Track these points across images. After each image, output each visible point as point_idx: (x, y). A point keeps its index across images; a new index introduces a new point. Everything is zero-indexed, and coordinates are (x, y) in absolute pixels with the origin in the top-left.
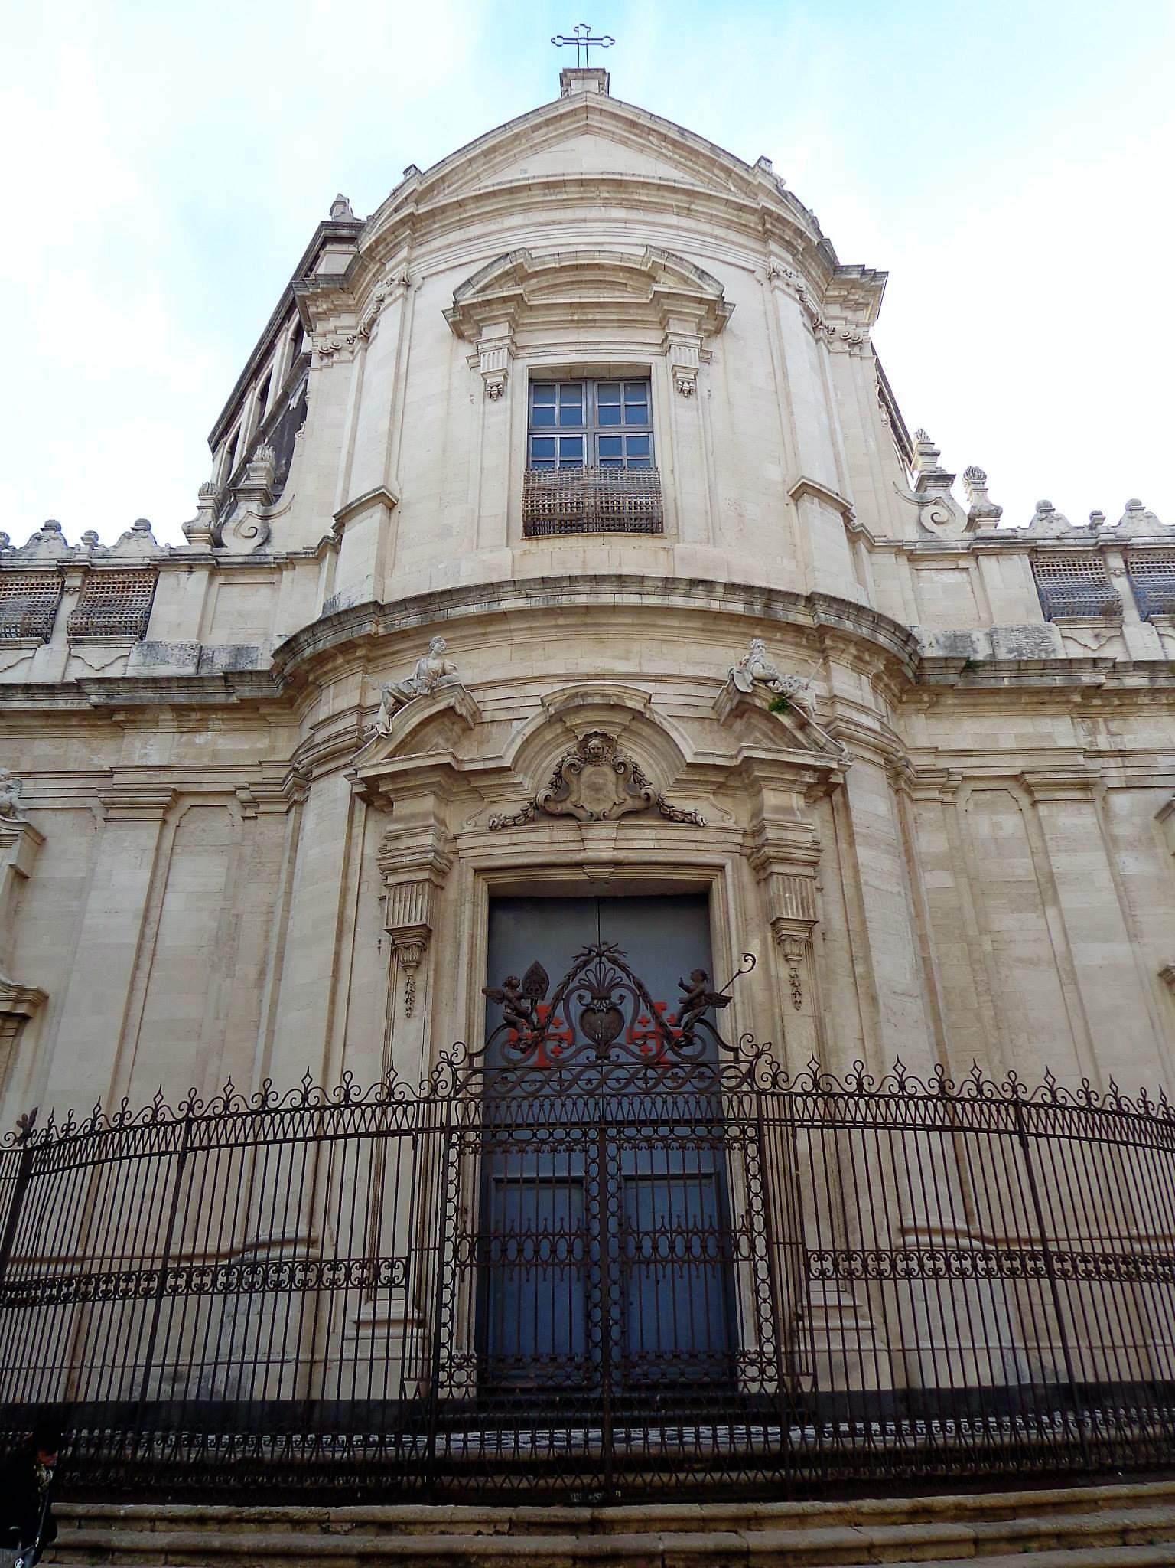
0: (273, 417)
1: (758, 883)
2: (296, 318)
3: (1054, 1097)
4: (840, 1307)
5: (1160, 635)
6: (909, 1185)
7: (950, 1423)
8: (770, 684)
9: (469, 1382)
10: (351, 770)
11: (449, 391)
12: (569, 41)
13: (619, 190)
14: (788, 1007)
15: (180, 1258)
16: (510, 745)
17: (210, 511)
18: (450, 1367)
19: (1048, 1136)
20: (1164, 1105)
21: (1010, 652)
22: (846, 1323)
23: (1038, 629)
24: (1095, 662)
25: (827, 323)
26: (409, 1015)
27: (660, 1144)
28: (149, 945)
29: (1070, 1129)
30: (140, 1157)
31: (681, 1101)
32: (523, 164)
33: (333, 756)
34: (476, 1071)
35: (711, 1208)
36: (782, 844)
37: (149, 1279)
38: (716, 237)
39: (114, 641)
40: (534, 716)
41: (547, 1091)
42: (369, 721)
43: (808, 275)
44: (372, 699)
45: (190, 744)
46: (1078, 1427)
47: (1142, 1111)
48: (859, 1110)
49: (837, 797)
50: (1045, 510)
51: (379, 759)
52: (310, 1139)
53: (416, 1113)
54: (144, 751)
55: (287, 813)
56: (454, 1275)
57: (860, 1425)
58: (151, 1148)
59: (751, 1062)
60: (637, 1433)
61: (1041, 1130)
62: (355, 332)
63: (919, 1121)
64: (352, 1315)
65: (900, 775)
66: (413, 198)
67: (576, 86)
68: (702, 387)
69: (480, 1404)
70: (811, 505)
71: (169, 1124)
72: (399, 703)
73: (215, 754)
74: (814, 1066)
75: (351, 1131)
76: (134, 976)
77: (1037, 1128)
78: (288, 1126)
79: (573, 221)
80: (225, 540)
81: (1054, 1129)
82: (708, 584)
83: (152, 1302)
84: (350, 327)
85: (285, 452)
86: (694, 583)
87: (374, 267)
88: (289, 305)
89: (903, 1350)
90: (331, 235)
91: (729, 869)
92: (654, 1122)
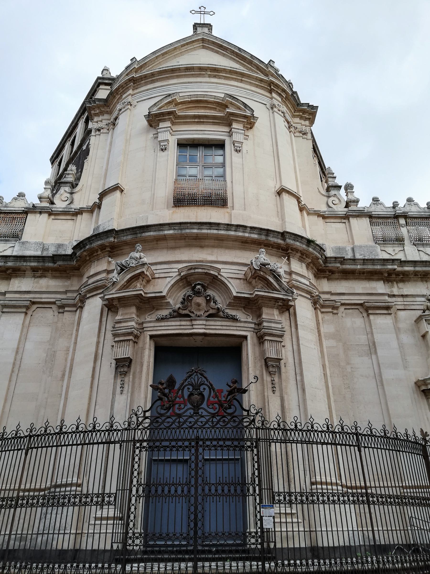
0: (76, 152)
1: (260, 343)
2: (86, 114)
3: (371, 432)
4: (280, 513)
5: (418, 250)
6: (327, 466)
7: (327, 561)
8: (267, 266)
9: (141, 544)
10: (102, 295)
11: (146, 147)
12: (197, 12)
13: (215, 71)
14: (270, 393)
15: (24, 490)
16: (165, 287)
17: (49, 190)
18: (133, 538)
19: (369, 448)
20: (414, 436)
21: (361, 255)
22: (288, 520)
23: (371, 247)
24: (393, 260)
25: (294, 125)
26: (121, 393)
27: (213, 448)
28: (18, 363)
29: (377, 445)
30: (10, 451)
31: (226, 431)
32: (178, 59)
33: (96, 289)
34: (147, 418)
35: (239, 474)
36: (269, 328)
37: (12, 501)
38: (252, 91)
39: (8, 240)
40: (174, 276)
41: (174, 426)
42: (111, 276)
43: (287, 107)
44: (113, 267)
45: (38, 282)
46: (377, 563)
47: (406, 438)
48: (296, 436)
49: (291, 310)
50: (376, 200)
51: (113, 291)
52: (79, 445)
53: (122, 434)
54: (20, 285)
55: (76, 311)
56: (136, 500)
57: (292, 562)
58: (14, 447)
59: (254, 416)
60: (207, 564)
61: (366, 445)
62: (109, 122)
63: (319, 441)
64: (93, 515)
65: (316, 302)
66: (134, 70)
67: (199, 30)
68: (245, 148)
69: (145, 552)
70: (285, 196)
71: (22, 437)
72: (122, 270)
73: (48, 286)
74: (278, 418)
75: (95, 441)
76: (11, 375)
77: (364, 444)
78: (70, 439)
79: (196, 82)
80: (55, 201)
81: (371, 445)
82: (245, 227)
83: (12, 510)
84: (108, 120)
85: (80, 168)
86: (238, 226)
87: (118, 97)
88: (83, 109)
89: (353, 531)
90: (99, 83)
91: (249, 338)
92: (175, 440)
